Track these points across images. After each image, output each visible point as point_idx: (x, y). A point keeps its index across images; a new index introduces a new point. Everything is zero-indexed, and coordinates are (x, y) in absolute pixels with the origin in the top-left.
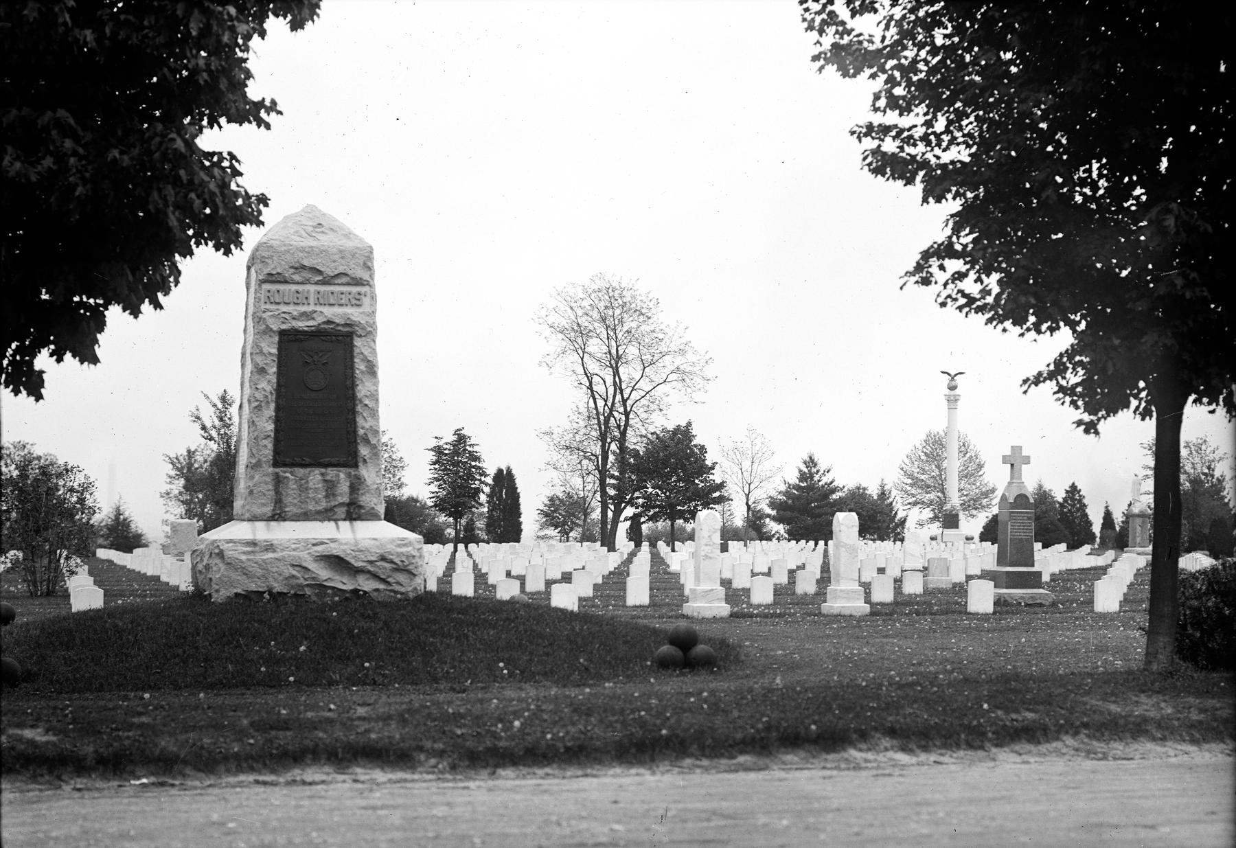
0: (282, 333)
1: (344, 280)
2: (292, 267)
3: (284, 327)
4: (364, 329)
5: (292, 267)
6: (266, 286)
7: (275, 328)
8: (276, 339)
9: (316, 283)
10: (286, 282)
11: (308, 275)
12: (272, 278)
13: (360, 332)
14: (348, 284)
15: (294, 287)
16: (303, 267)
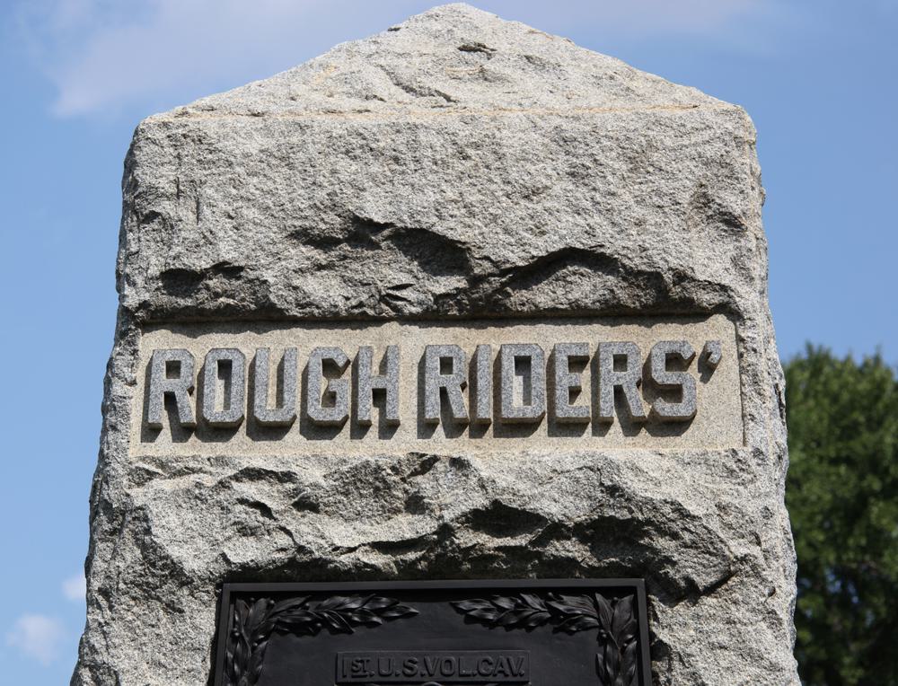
0: (237, 586)
1: (586, 287)
3: (246, 552)
4: (707, 546)
6: (158, 343)
7: (195, 559)
8: (202, 620)
9: (432, 316)
10: (267, 317)
11: (393, 270)
12: (191, 301)
13: (691, 567)
14: (611, 313)
15: (308, 345)
16: (362, 233)
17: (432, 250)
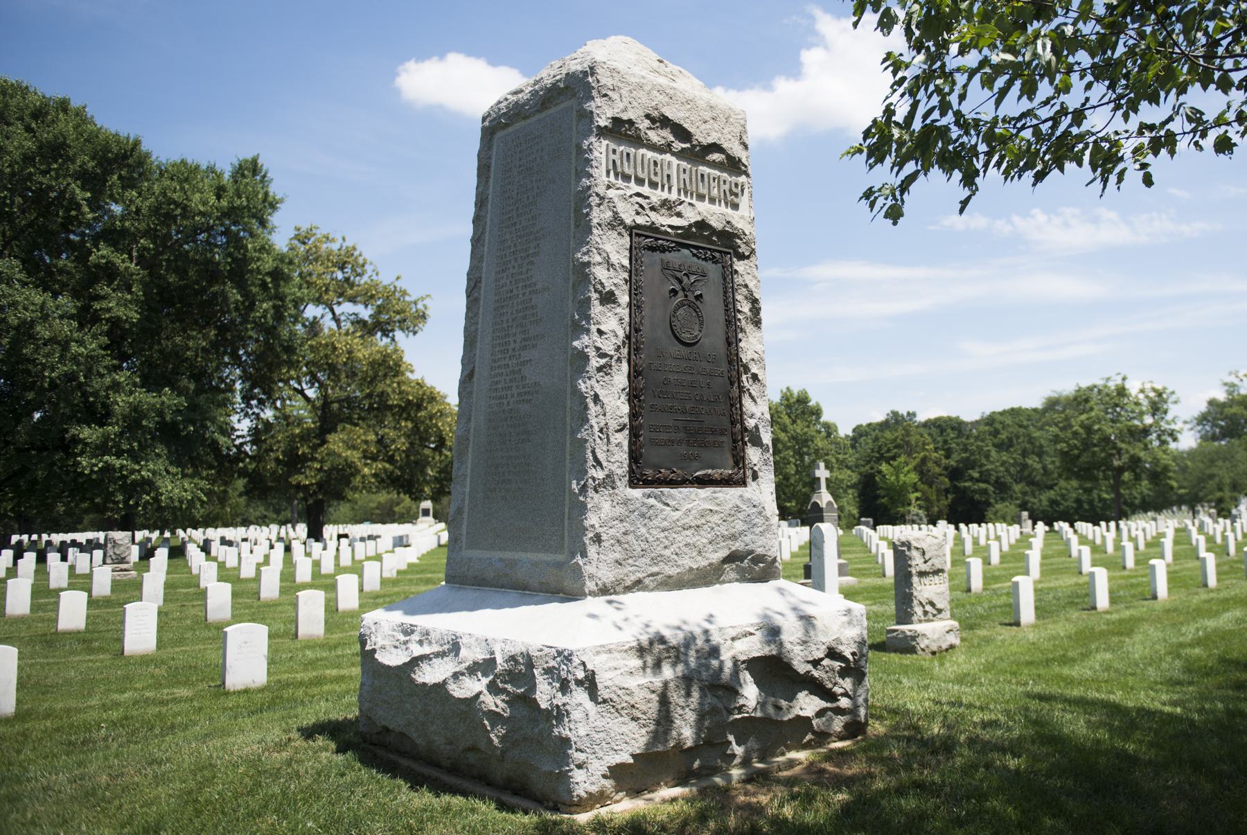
2: (648, 116)
5: (648, 116)
13: (743, 249)
17: (682, 133)
